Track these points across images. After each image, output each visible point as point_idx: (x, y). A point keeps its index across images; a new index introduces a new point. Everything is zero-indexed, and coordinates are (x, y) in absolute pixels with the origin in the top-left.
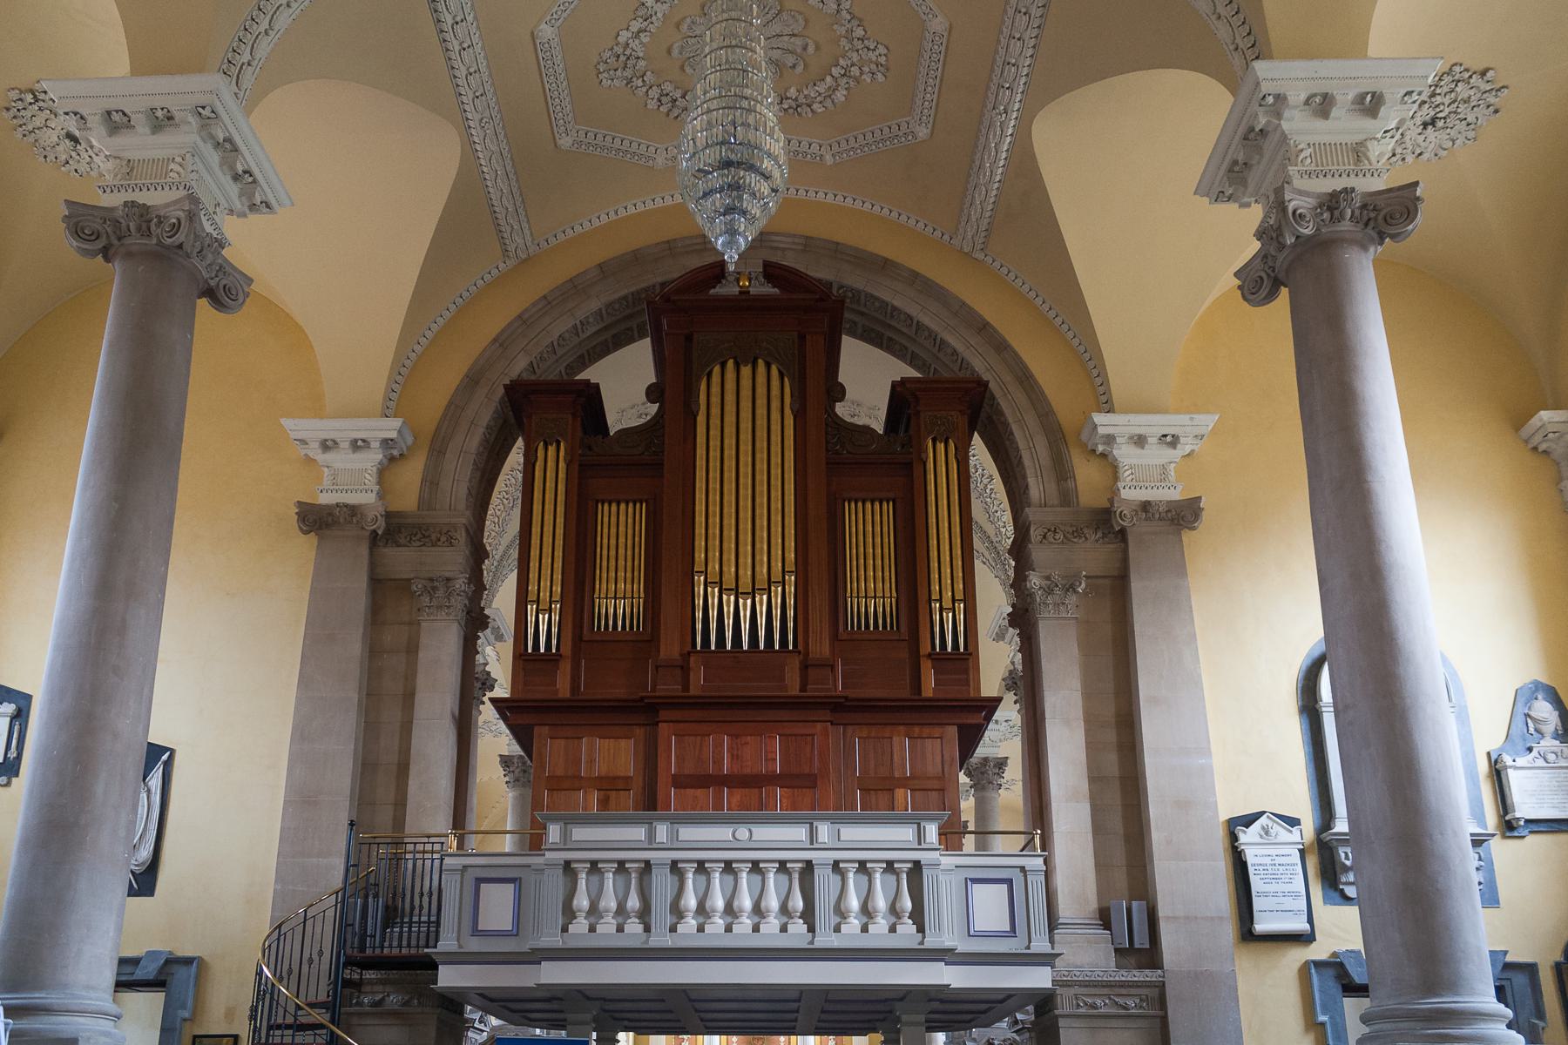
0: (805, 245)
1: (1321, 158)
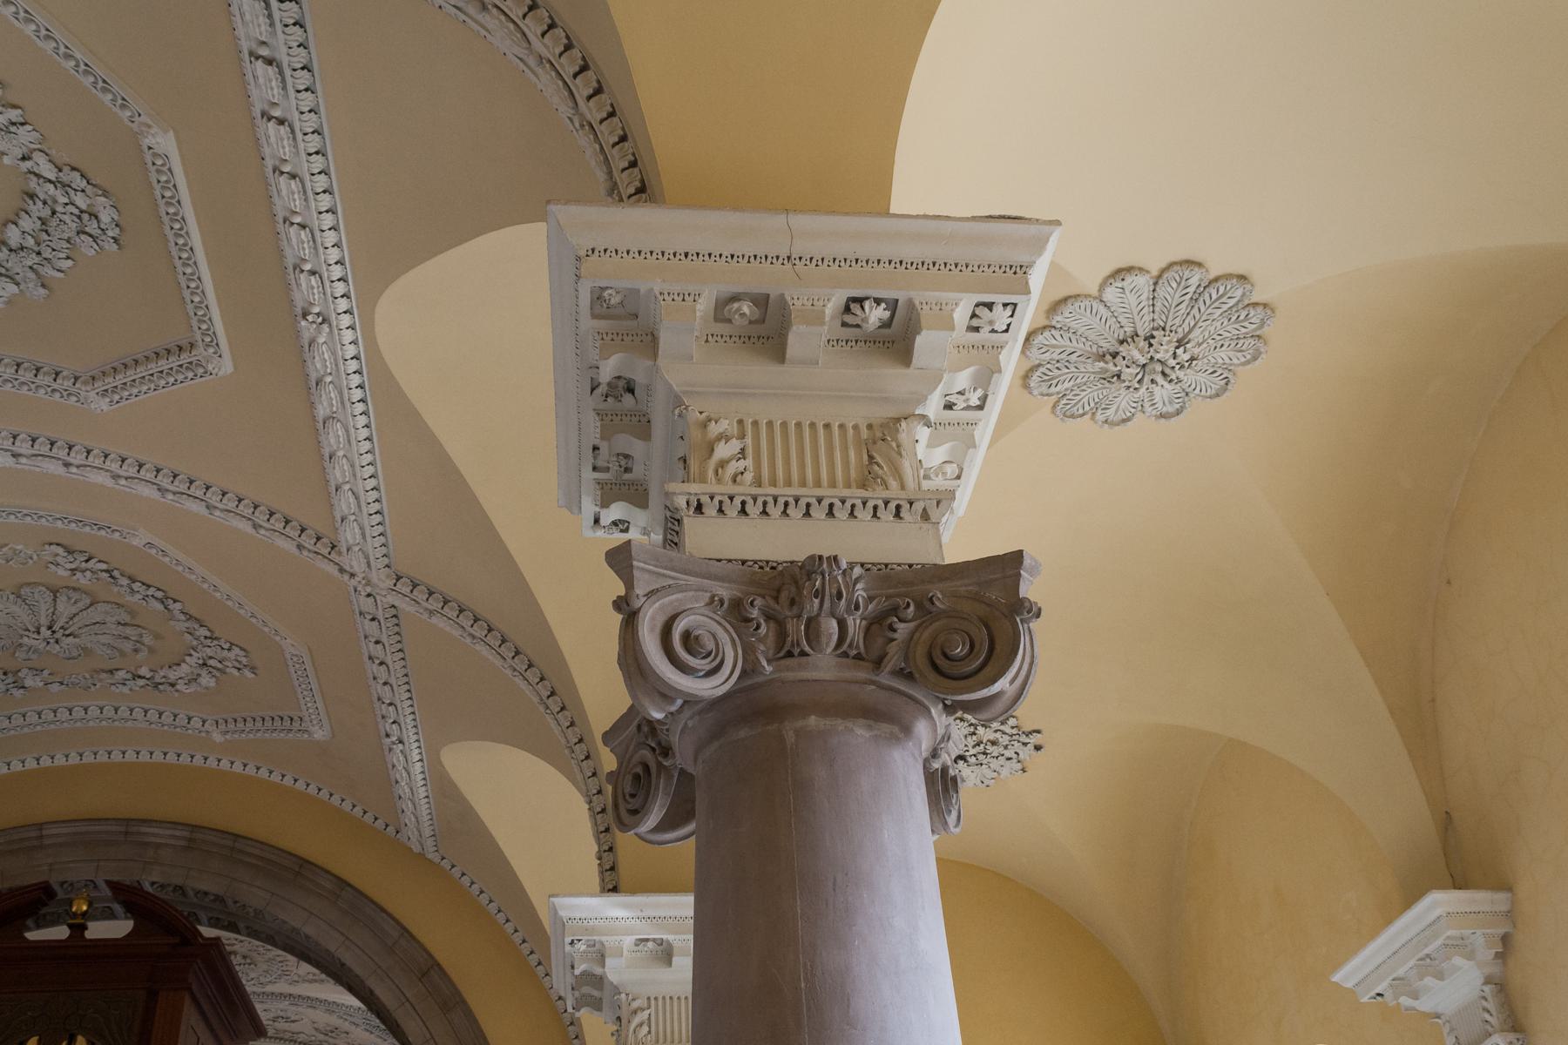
0: (41, 829)
1: (802, 466)
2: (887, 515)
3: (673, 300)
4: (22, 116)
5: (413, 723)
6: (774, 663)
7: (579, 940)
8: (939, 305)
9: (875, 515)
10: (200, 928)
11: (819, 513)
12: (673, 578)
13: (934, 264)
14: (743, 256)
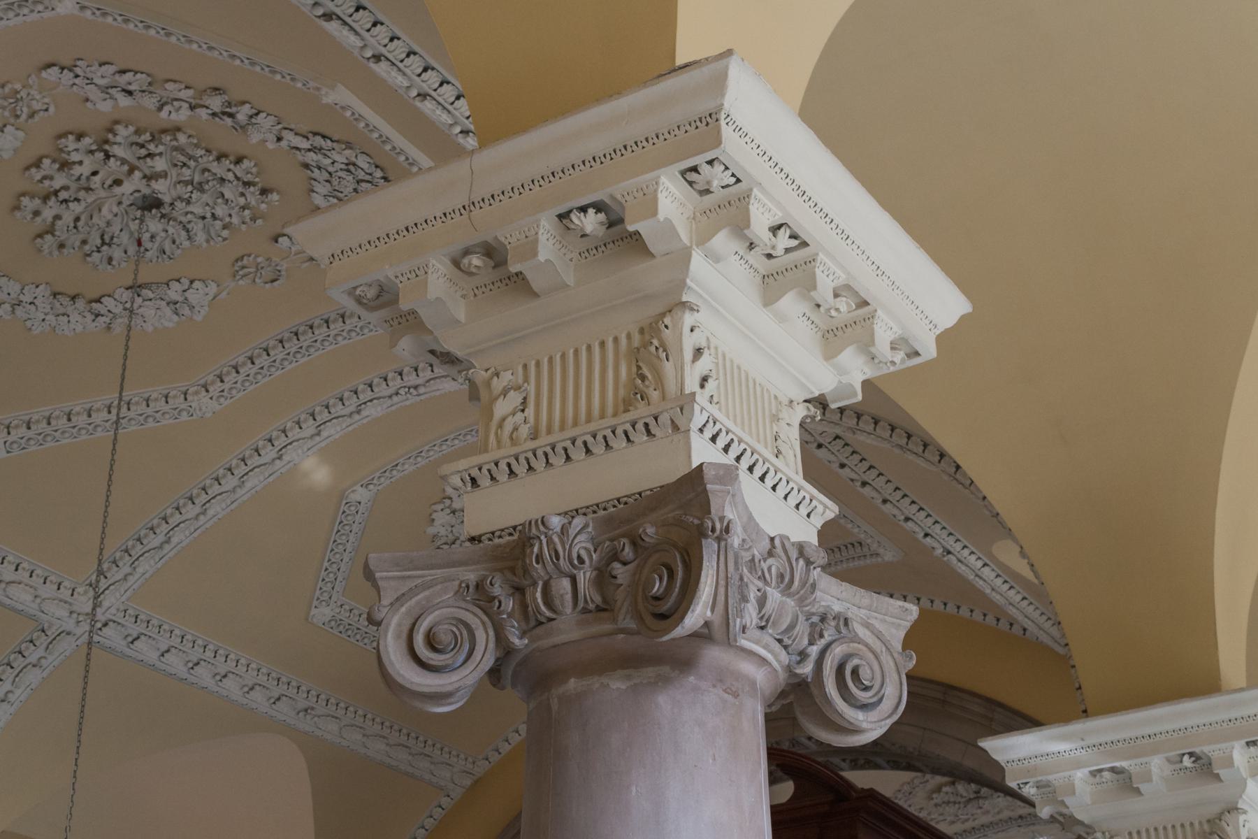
2: (640, 437)
3: (409, 279)
4: (252, 108)
5: (945, 533)
6: (528, 635)
7: (1026, 783)
8: (640, 190)
9: (628, 440)
10: (844, 774)
11: (578, 454)
12: (419, 577)
13: (625, 147)
14: (454, 211)
